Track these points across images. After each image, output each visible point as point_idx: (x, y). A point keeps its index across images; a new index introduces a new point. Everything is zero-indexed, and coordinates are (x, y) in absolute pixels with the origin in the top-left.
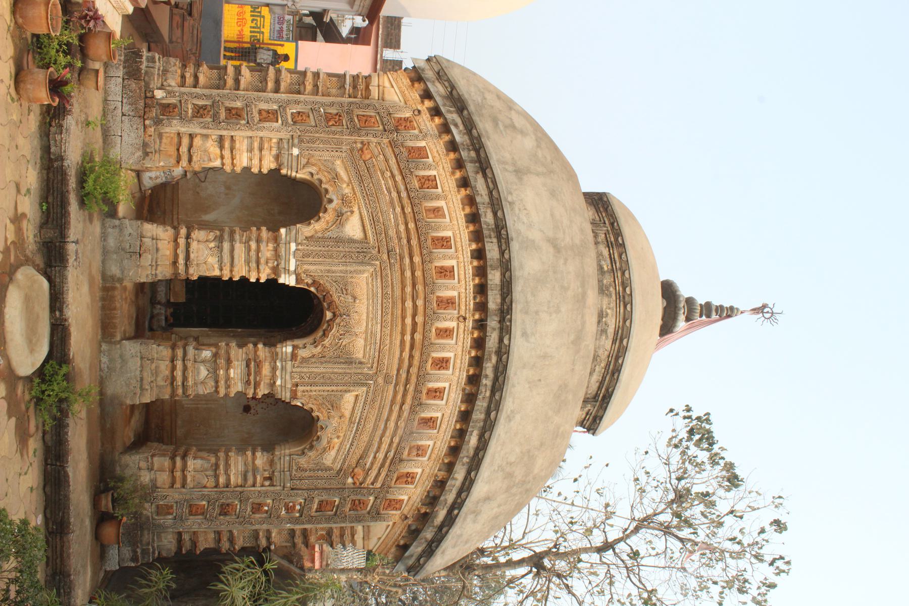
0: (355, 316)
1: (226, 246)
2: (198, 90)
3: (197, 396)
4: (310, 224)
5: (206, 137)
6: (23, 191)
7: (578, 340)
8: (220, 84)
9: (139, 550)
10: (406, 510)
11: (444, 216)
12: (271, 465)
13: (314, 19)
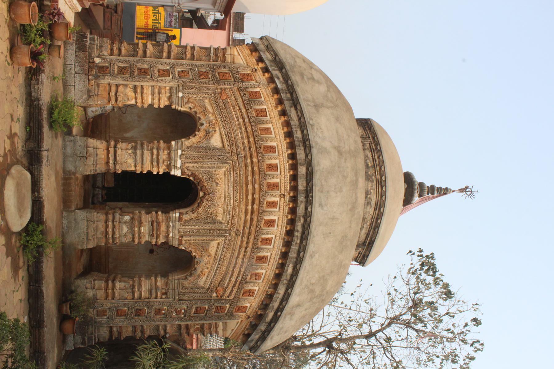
1: (139, 152)
2: (121, 58)
4: (189, 138)
5: (126, 86)
6: (15, 119)
7: (353, 208)
8: (134, 54)
10: (249, 312)
11: (271, 134)
12: (166, 286)
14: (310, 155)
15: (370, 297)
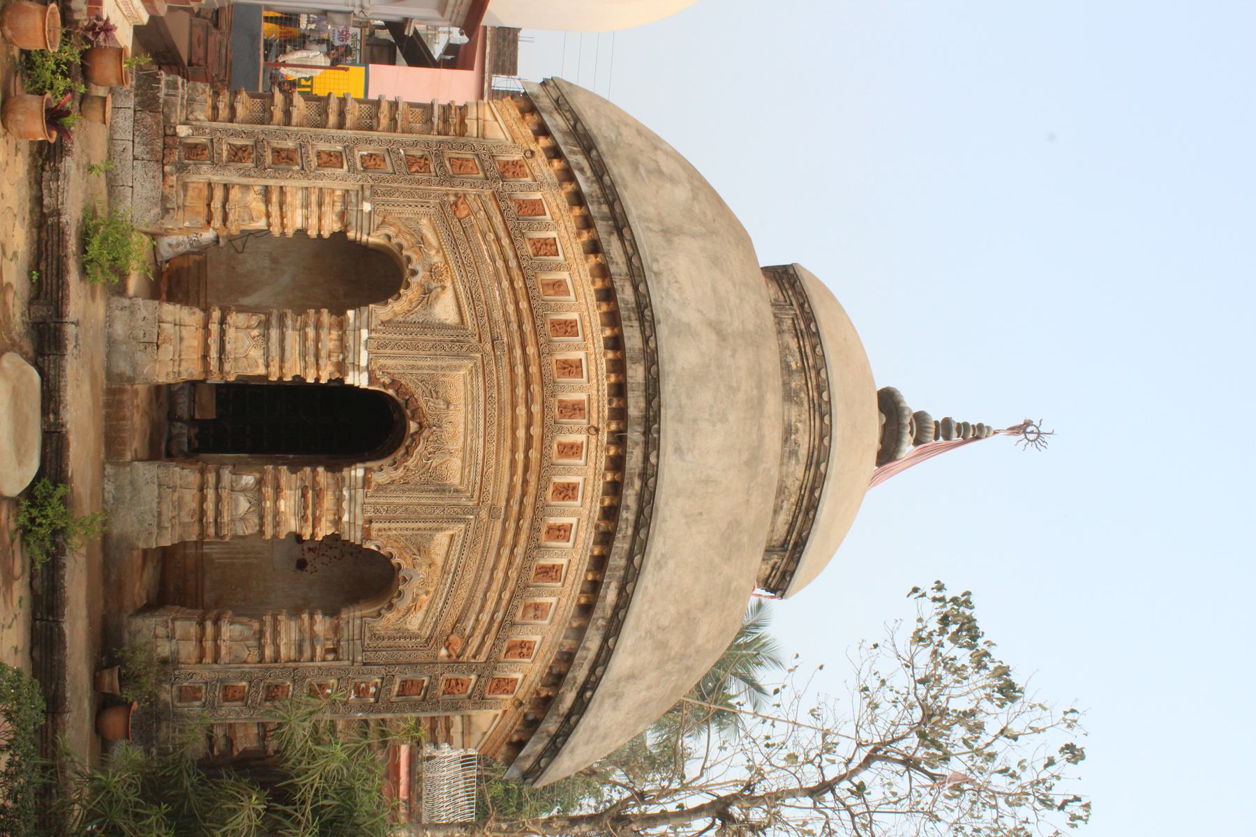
0: (450, 428)
1: (274, 333)
2: (235, 126)
3: (235, 537)
4: (386, 304)
5: (246, 187)
6: (9, 254)
8: (265, 117)
9: (154, 750)
10: (520, 693)
11: (568, 293)
14: (652, 338)
15: (821, 699)
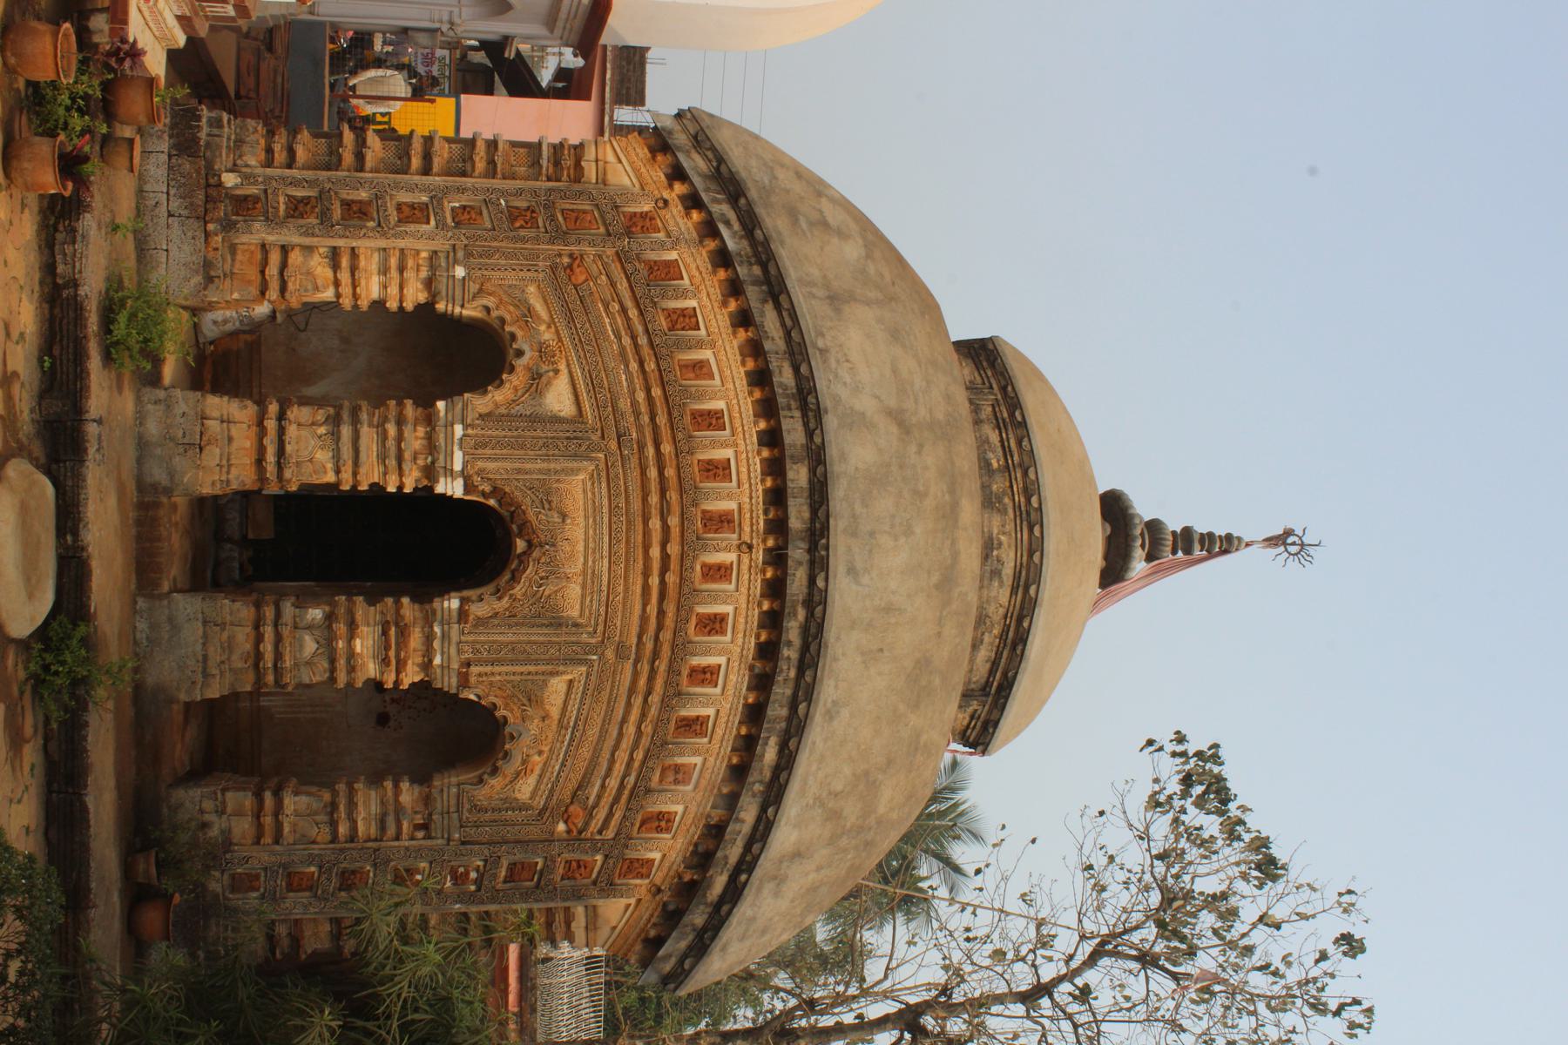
1: (346, 431)
2: (294, 172)
3: (300, 685)
4: (485, 392)
5: (309, 250)
6: (15, 335)
7: (947, 582)
8: (333, 163)
9: (201, 954)
10: (658, 876)
12: (426, 805)
13: (489, 55)
15: (1034, 881)
